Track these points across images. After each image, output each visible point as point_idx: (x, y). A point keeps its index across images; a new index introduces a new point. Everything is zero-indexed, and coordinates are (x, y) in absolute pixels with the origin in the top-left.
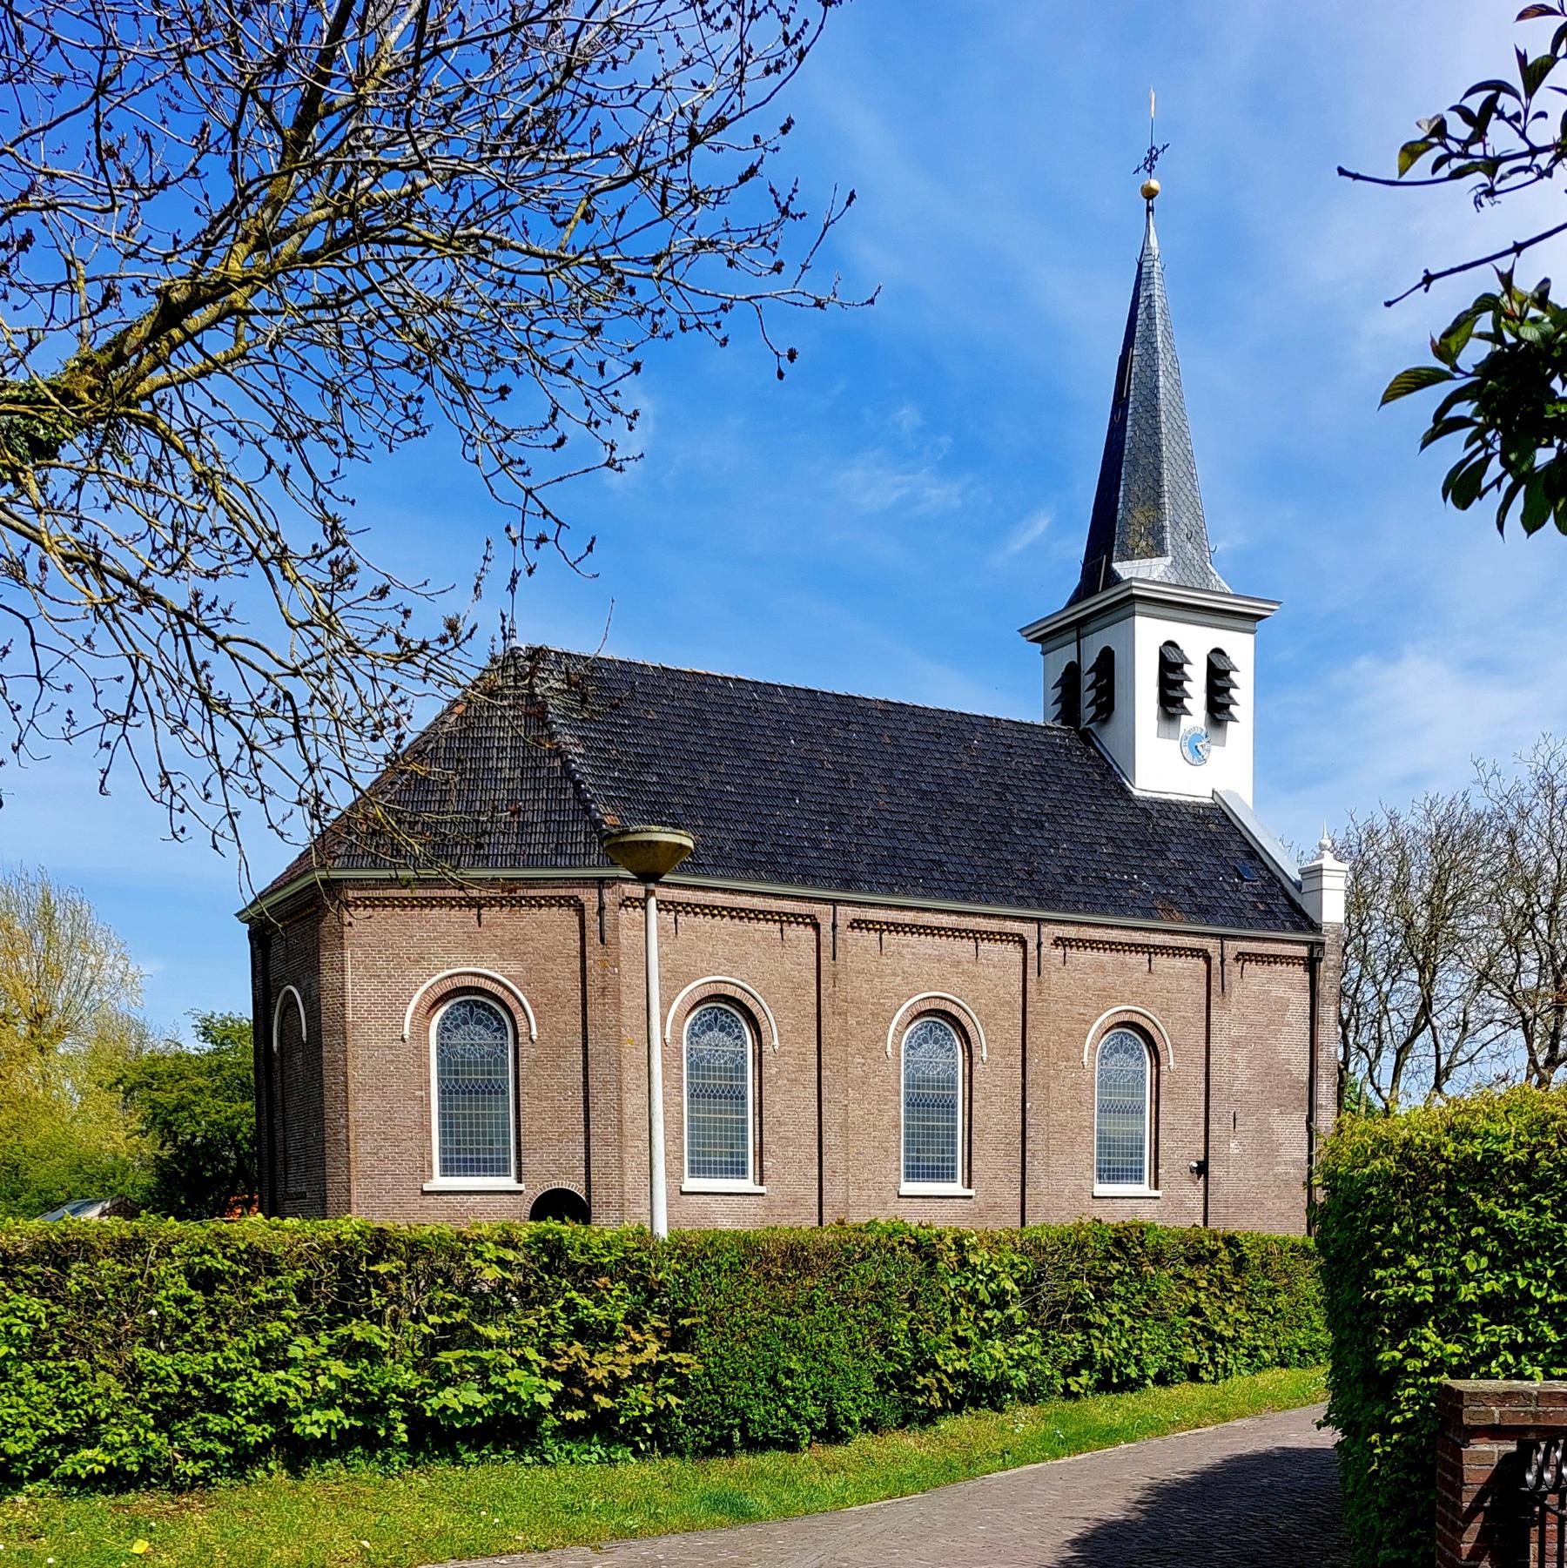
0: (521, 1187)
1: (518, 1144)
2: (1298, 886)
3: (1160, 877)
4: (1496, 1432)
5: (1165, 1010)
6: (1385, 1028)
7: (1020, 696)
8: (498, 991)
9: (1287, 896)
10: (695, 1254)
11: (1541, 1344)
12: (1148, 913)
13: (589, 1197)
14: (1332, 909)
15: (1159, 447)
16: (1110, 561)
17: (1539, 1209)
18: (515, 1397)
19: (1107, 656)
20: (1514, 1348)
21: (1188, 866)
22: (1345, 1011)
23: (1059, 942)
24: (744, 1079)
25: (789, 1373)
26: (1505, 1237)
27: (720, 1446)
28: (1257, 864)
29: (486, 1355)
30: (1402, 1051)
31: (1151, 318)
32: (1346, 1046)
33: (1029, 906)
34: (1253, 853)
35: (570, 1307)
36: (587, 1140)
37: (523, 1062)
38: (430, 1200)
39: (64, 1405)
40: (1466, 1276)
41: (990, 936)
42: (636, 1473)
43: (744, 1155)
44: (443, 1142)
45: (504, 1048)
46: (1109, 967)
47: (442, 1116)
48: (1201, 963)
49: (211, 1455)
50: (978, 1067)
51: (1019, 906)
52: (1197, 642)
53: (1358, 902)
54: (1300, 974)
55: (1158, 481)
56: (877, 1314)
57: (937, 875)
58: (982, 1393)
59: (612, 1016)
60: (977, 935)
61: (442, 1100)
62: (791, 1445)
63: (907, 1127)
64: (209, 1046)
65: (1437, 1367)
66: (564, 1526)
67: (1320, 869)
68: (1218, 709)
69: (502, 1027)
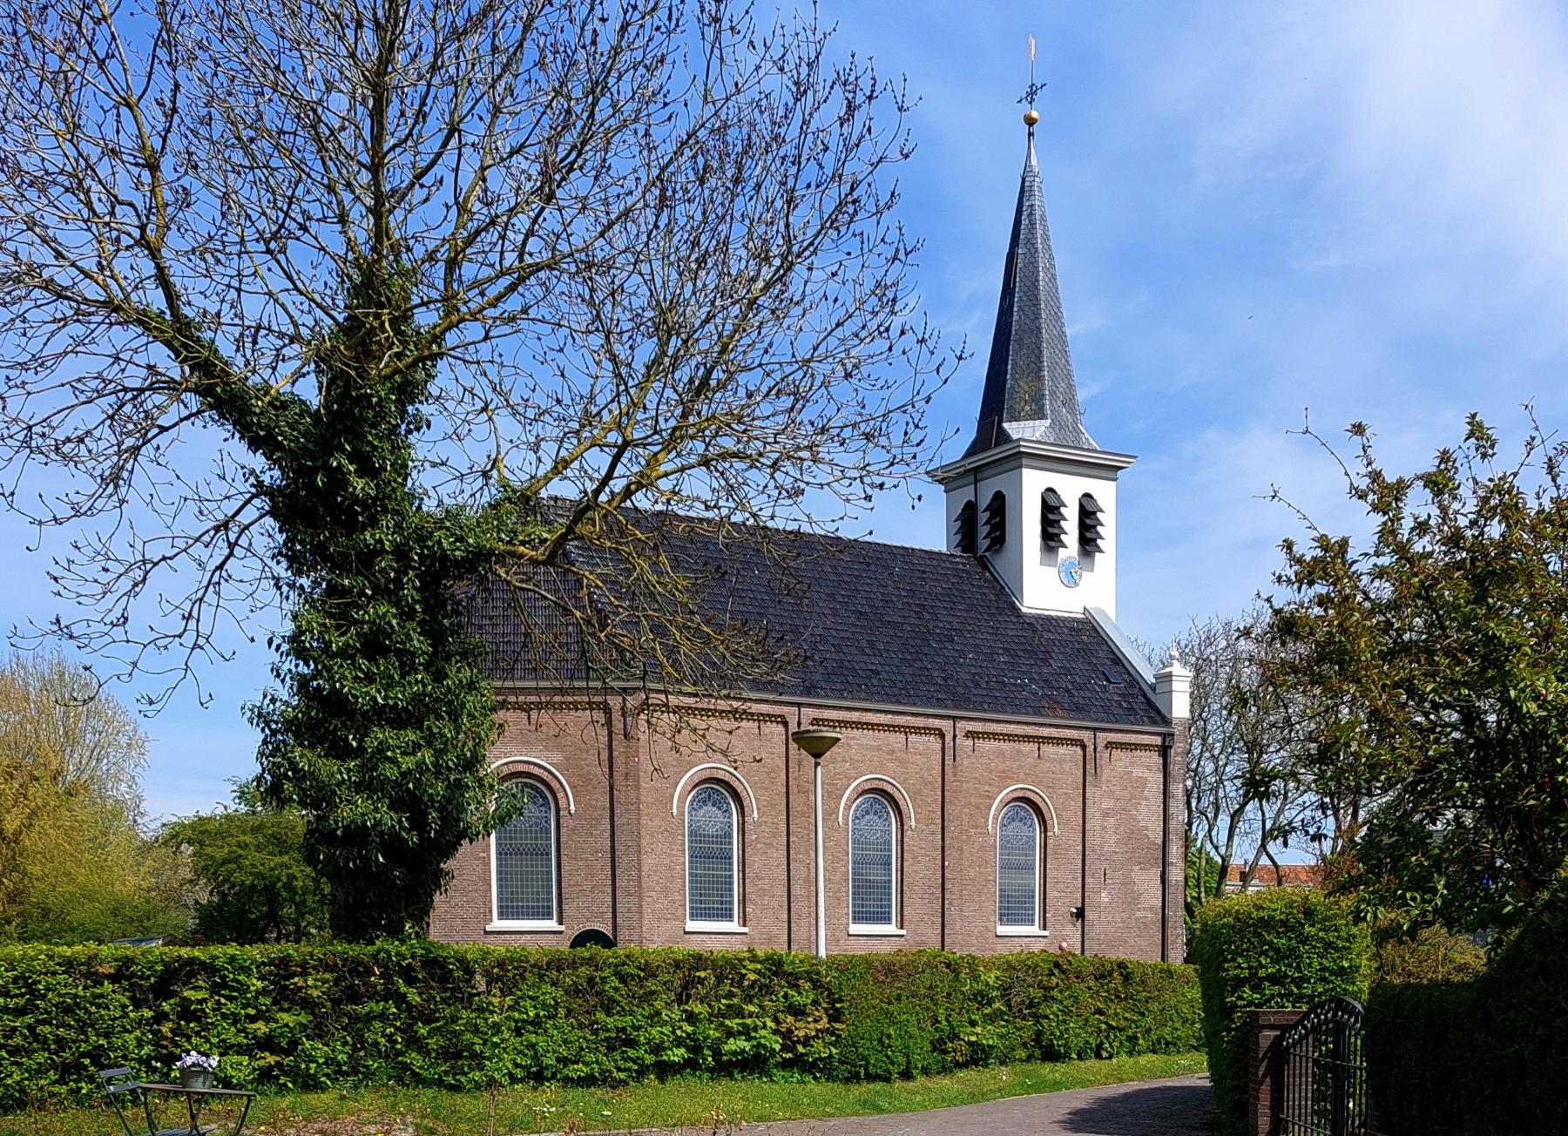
0: (562, 928)
1: (560, 894)
2: (1153, 687)
3: (1046, 681)
4: (1272, 1027)
5: (1051, 788)
6: (1221, 794)
7: (920, 523)
8: (545, 775)
9: (1144, 695)
10: (844, 966)
11: (1291, 994)
12: (1037, 713)
13: (615, 936)
14: (1180, 707)
15: (1039, 329)
16: (1001, 421)
17: (1290, 939)
18: (764, 1046)
19: (999, 497)
20: (1280, 995)
21: (1067, 671)
22: (1189, 783)
23: (971, 735)
24: (731, 843)
25: (889, 1036)
26: (1278, 951)
27: (853, 1078)
28: (1120, 669)
29: (749, 1021)
30: (1235, 816)
31: (1032, 224)
32: (1190, 812)
33: (946, 707)
34: (1117, 660)
35: (786, 996)
36: (614, 891)
37: (563, 830)
38: (491, 938)
39: (565, 1042)
40: (1261, 966)
41: (917, 730)
42: (817, 1088)
43: (731, 903)
44: (500, 893)
45: (548, 821)
46: (1008, 754)
47: (499, 872)
48: (1079, 750)
49: (628, 1070)
50: (908, 833)
51: (940, 707)
52: (1071, 488)
53: (1199, 697)
54: (1156, 759)
55: (1039, 358)
56: (930, 1005)
57: (875, 682)
58: (978, 1057)
59: (633, 795)
60: (908, 730)
61: (498, 859)
62: (887, 1079)
63: (854, 880)
64: (243, 809)
65: (1250, 1003)
66: (797, 1112)
67: (1170, 675)
68: (1088, 541)
69: (546, 804)
